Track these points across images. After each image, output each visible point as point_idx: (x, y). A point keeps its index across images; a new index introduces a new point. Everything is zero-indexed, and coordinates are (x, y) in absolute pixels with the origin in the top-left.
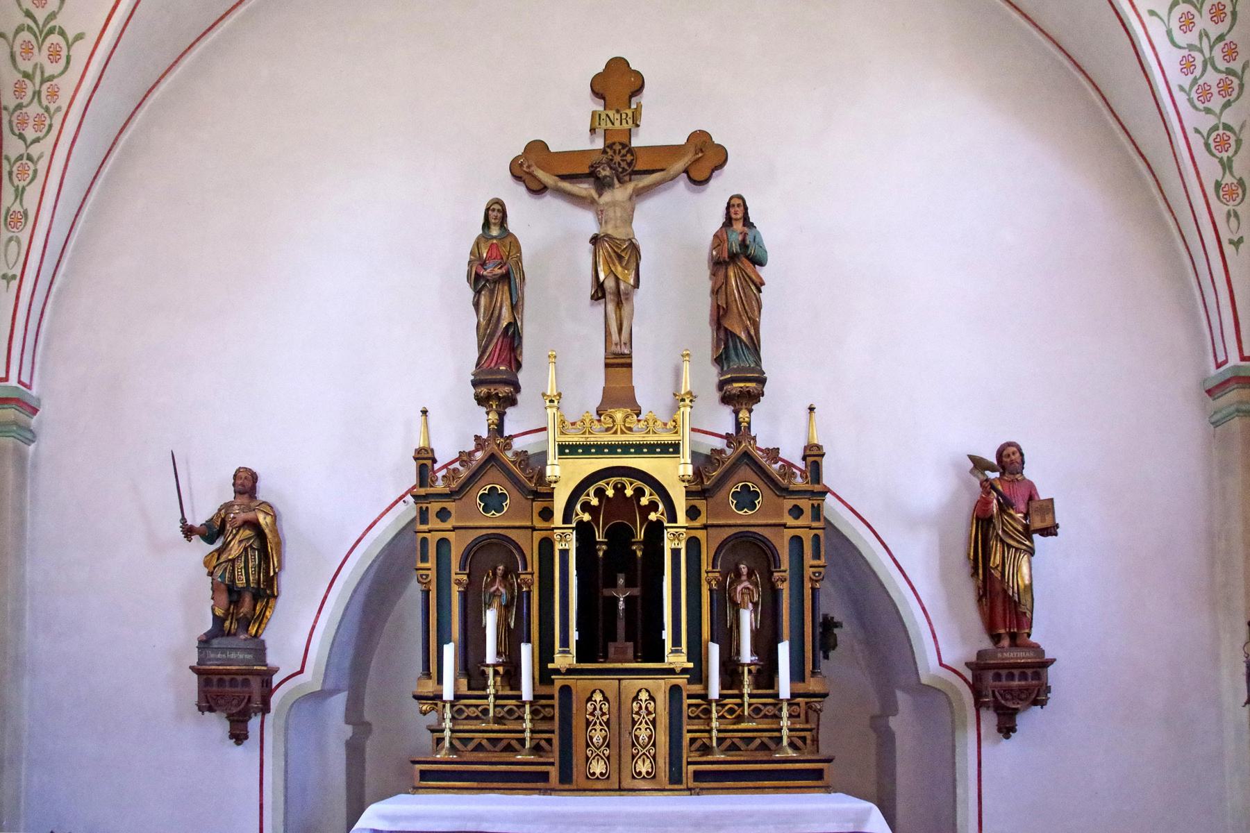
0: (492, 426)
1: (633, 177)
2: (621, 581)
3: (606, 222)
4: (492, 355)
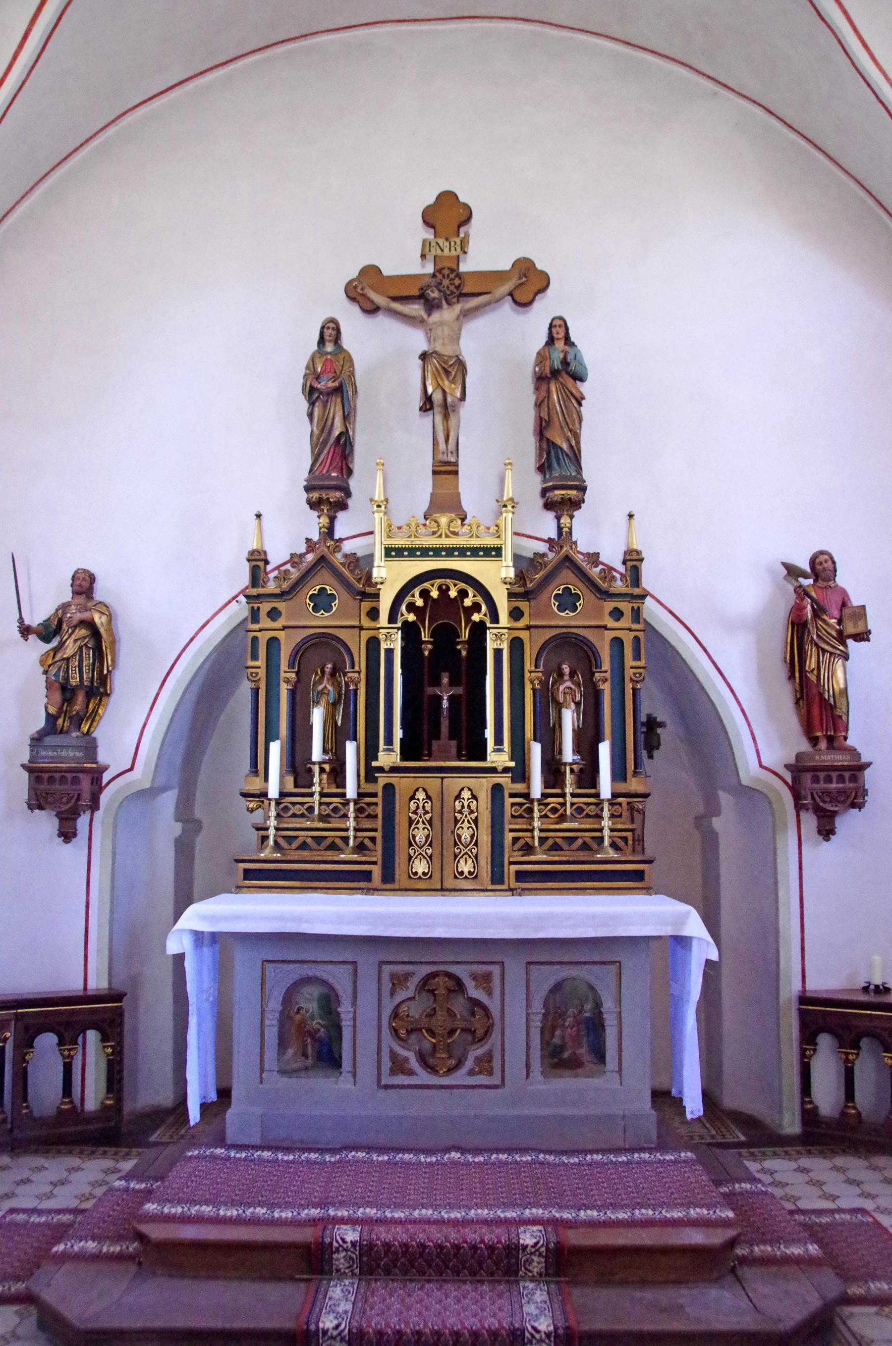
0: (323, 529)
1: (461, 299)
2: (445, 680)
3: (434, 340)
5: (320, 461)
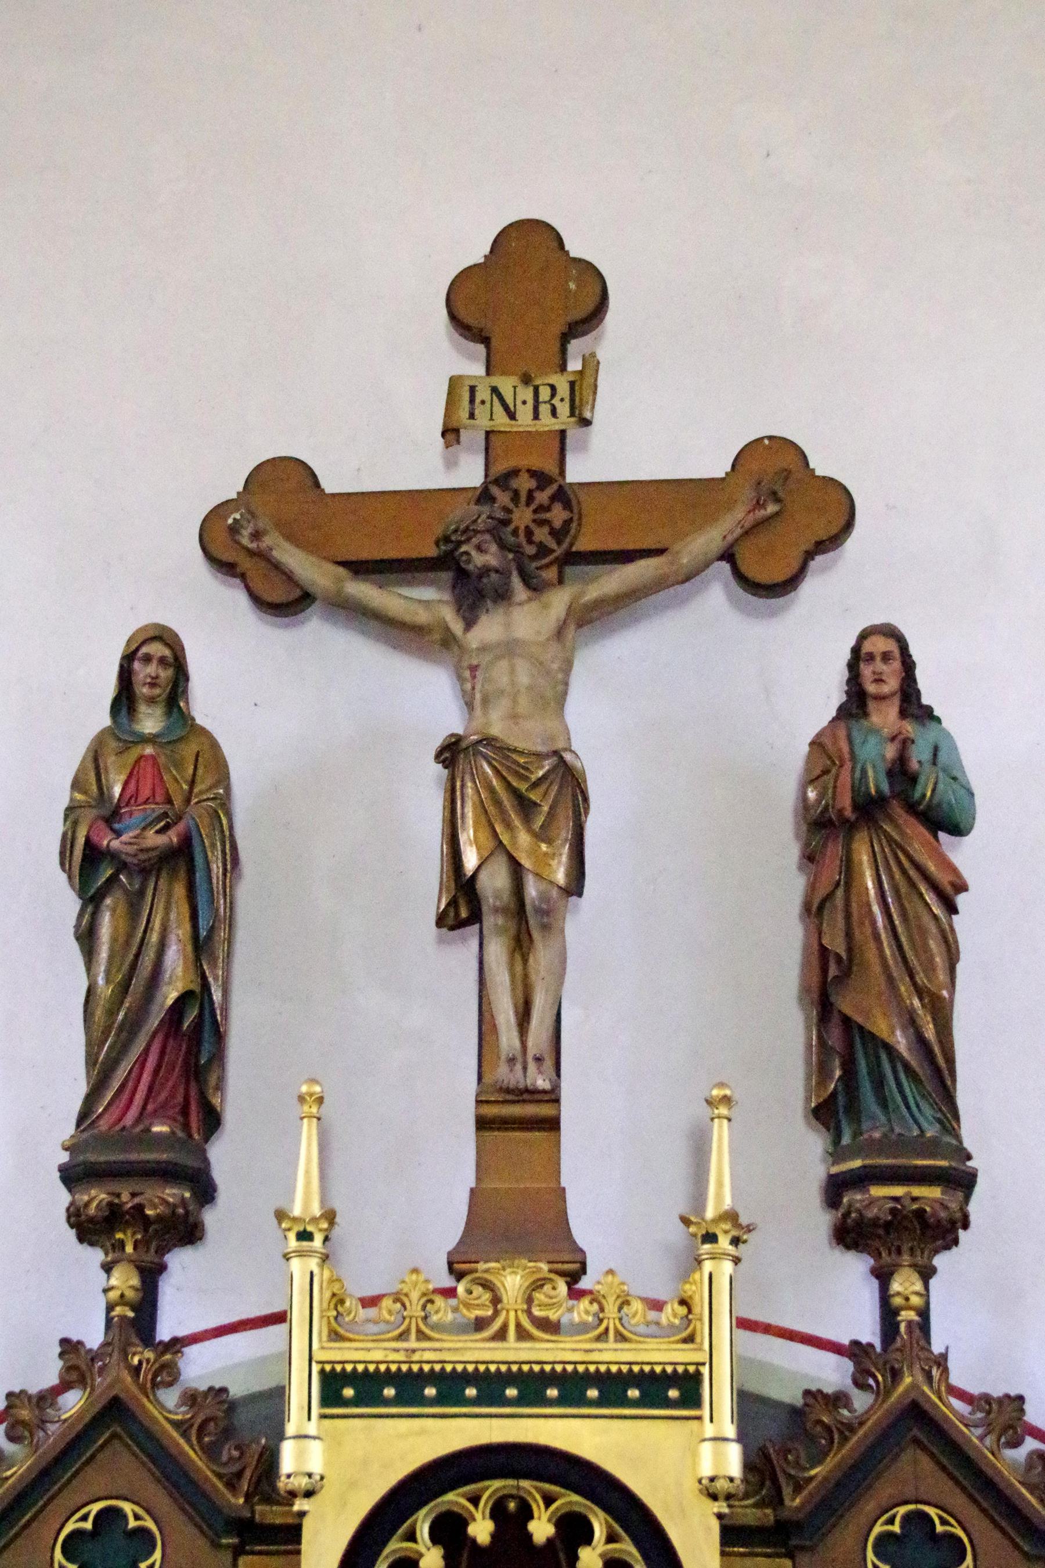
0: (118, 1310)
1: (569, 570)
3: (486, 701)
4: (130, 1084)
5: (115, 1085)
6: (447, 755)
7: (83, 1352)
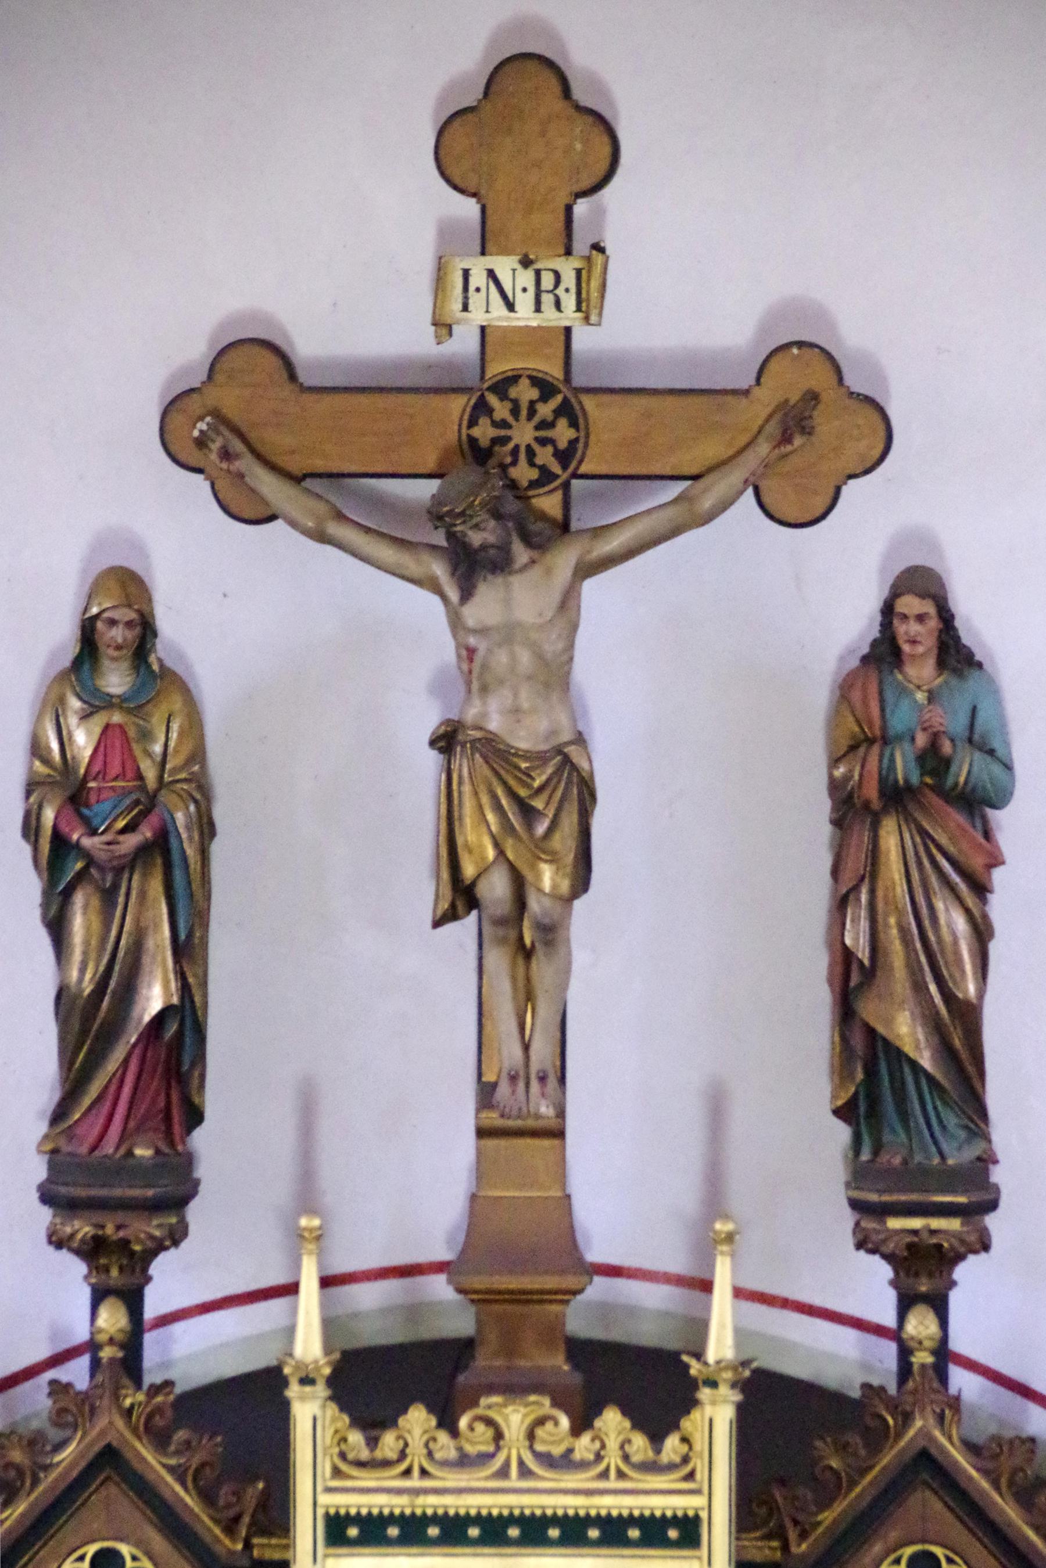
3: (484, 689)
6: (442, 744)
7: (71, 1392)
